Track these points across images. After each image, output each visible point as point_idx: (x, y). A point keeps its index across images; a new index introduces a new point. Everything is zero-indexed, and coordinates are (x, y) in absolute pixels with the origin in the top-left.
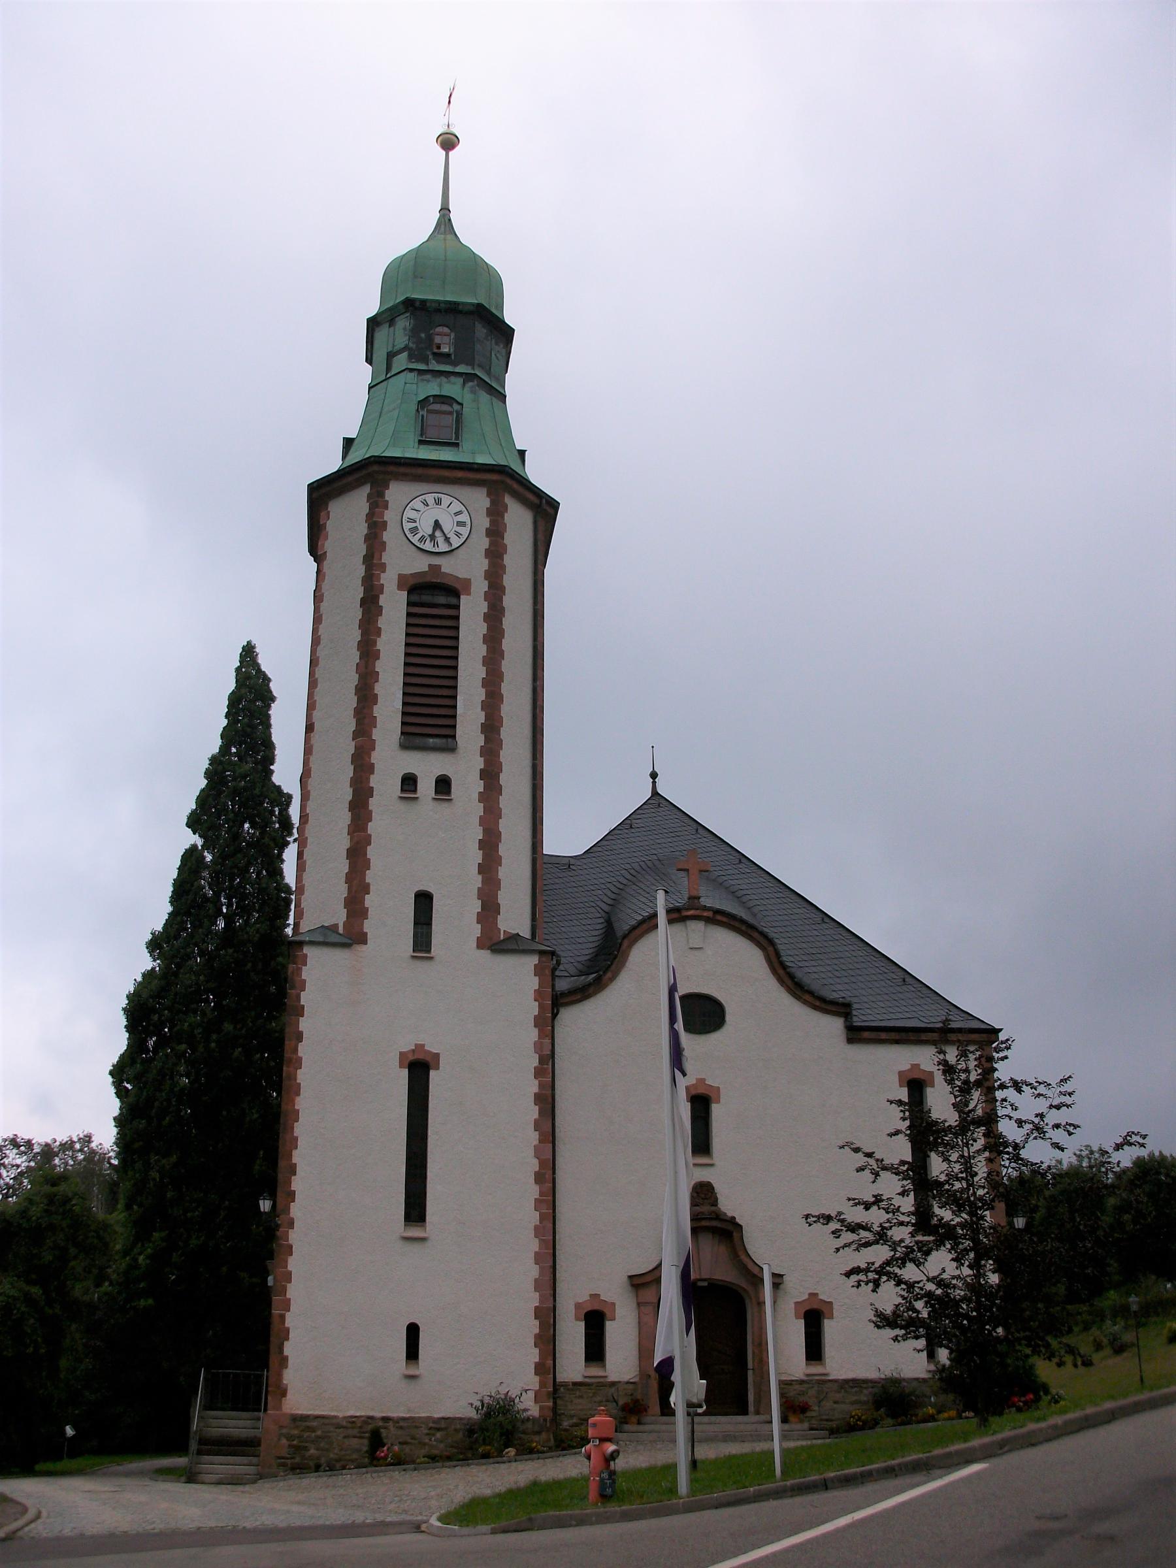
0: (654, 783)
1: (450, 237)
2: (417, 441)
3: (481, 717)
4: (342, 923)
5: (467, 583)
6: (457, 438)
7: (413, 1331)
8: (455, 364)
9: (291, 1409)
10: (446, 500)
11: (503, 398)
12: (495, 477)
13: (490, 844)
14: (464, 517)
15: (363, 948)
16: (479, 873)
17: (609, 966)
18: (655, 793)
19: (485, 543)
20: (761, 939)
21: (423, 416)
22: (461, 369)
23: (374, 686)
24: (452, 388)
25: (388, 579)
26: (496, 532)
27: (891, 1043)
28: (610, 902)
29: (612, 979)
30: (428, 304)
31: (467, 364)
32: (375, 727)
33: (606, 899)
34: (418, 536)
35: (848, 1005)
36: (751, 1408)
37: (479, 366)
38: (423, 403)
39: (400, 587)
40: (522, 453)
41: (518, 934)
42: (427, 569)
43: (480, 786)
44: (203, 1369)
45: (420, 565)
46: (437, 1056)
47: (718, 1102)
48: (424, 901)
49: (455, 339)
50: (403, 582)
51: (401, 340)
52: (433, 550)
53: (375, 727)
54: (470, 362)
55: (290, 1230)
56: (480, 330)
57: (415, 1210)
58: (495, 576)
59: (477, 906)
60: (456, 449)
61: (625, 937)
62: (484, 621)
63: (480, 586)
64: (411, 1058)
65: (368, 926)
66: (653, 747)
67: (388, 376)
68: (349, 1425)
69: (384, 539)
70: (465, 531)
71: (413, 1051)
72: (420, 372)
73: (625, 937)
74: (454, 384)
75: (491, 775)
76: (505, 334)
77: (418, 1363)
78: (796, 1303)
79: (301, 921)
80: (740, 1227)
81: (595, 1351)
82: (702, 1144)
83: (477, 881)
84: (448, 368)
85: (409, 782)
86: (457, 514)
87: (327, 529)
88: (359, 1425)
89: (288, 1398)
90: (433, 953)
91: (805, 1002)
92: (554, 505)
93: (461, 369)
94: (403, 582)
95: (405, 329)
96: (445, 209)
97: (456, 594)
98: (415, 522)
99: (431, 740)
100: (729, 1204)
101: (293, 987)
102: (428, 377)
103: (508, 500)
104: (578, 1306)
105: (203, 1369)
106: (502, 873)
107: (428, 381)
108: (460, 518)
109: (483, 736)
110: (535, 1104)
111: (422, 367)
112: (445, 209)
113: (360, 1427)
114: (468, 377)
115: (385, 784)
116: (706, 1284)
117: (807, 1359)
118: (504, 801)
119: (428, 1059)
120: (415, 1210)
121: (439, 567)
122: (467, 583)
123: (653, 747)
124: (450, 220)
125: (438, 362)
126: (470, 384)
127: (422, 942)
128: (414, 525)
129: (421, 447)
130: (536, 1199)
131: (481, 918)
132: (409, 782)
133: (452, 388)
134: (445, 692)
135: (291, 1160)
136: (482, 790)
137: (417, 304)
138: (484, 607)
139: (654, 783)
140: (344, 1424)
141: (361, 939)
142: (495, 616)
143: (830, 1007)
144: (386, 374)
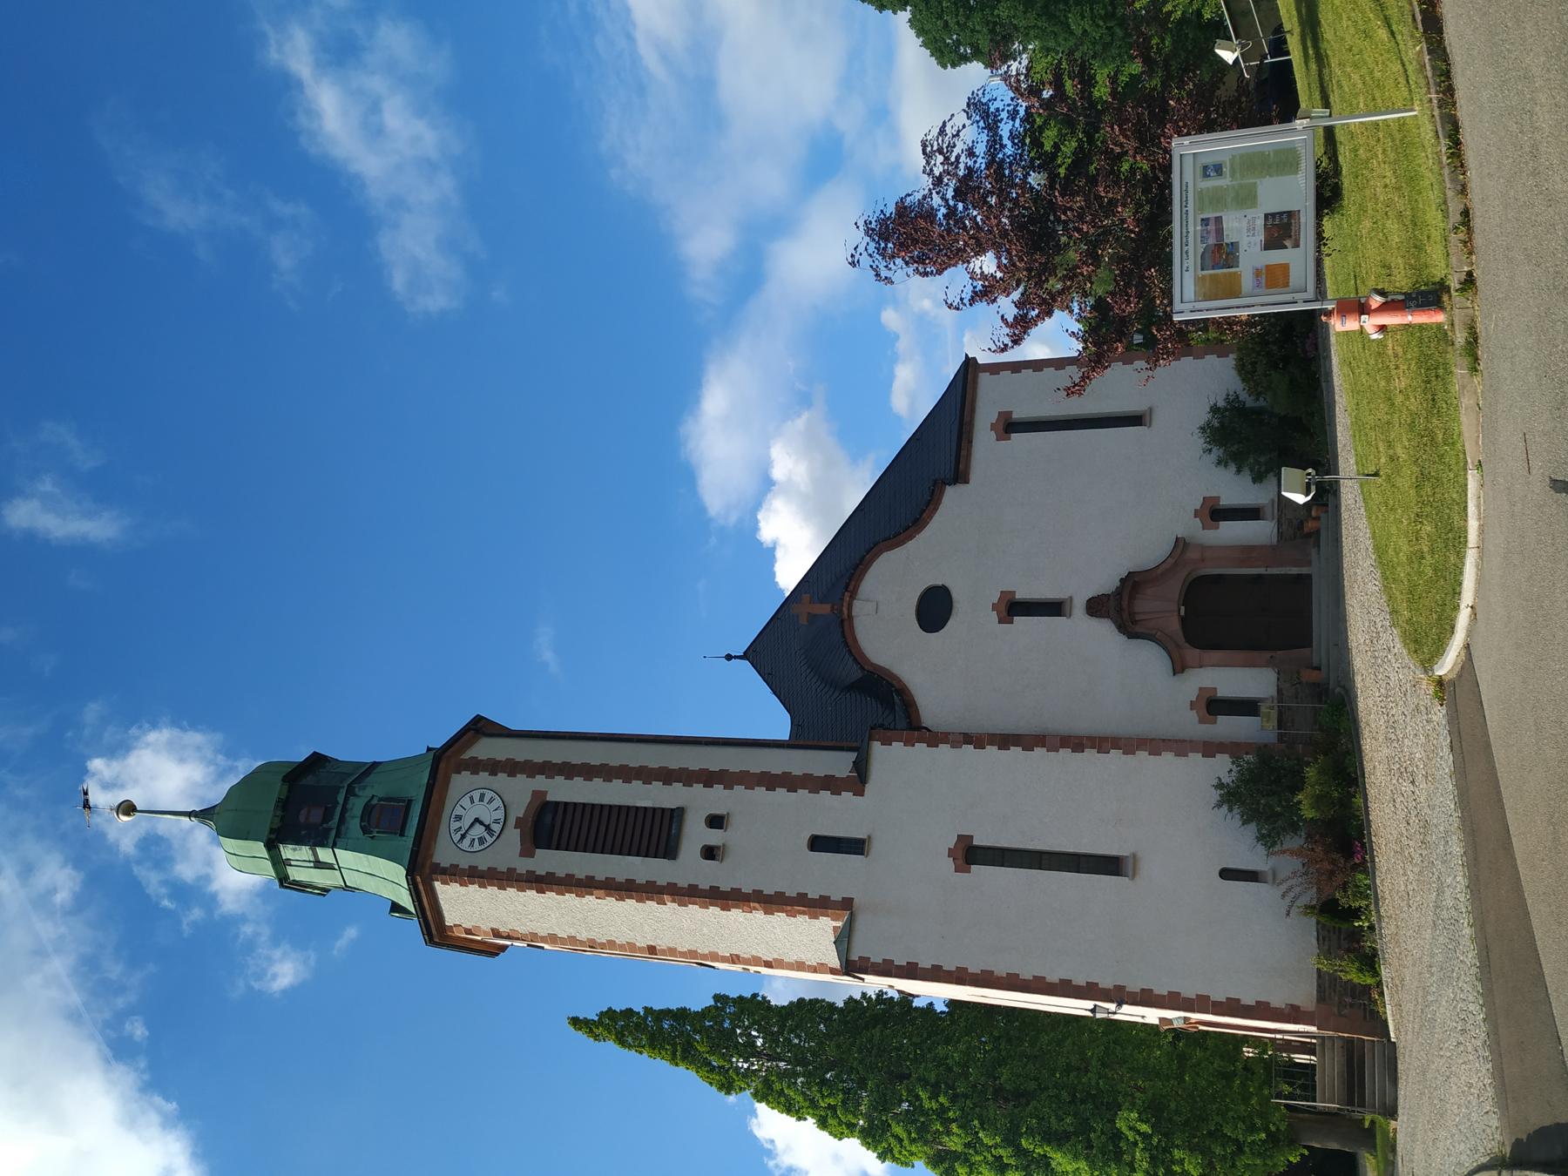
0: (736, 657)
1: (216, 810)
2: (399, 838)
3: (657, 785)
4: (832, 922)
6: (404, 801)
7: (1226, 874)
9: (1312, 1002)
10: (458, 811)
11: (375, 765)
12: (442, 765)
13: (770, 781)
14: (476, 795)
17: (887, 681)
18: (745, 656)
19: (502, 776)
21: (378, 832)
22: (341, 798)
23: (619, 882)
24: (357, 806)
25: (523, 865)
26: (494, 767)
27: (971, 446)
28: (832, 690)
30: (274, 827)
31: (338, 793)
32: (655, 882)
33: (830, 693)
34: (487, 837)
35: (935, 482)
36: (1304, 570)
37: (341, 782)
38: (365, 830)
40: (429, 749)
41: (854, 762)
42: (519, 830)
43: (719, 788)
45: (513, 835)
48: (819, 844)
50: (526, 852)
51: (304, 853)
52: (502, 824)
53: (655, 882)
54: (337, 790)
55: (1127, 989)
56: (309, 780)
57: (1110, 865)
59: (825, 794)
60: (414, 802)
61: (862, 668)
62: (572, 779)
63: (540, 782)
64: (960, 862)
66: (969, 854)
67: (336, 867)
68: (1326, 943)
69: (486, 869)
70: (489, 794)
73: (862, 668)
74: (354, 804)
75: (709, 778)
76: (317, 760)
77: (1261, 872)
78: (1204, 529)
79: (807, 963)
80: (1130, 573)
81: (1246, 707)
82: (1054, 608)
83: (803, 793)
84: (339, 809)
85: (710, 853)
86: (472, 801)
87: (470, 927)
88: (1326, 933)
89: (1300, 1004)
90: (865, 837)
92: (478, 719)
94: (526, 852)
96: (189, 814)
98: (474, 839)
99: (673, 831)
100: (1104, 581)
102: (343, 828)
103: (467, 756)
104: (1201, 721)
106: (797, 772)
107: (348, 828)
108: (476, 799)
109: (674, 784)
111: (333, 833)
112: (189, 814)
113: (1329, 931)
114: (351, 792)
116: (1183, 608)
117: (1258, 519)
118: (734, 769)
120: (1110, 865)
121: (518, 818)
123: (969, 854)
124: (201, 811)
125: (332, 819)
126: (357, 790)
127: (856, 847)
128: (477, 840)
129: (406, 834)
130: (1098, 752)
131: (836, 792)
132: (710, 853)
133: (357, 806)
134: (623, 817)
135: (1083, 986)
136: (722, 786)
137: (273, 836)
138: (559, 779)
139: (736, 657)
140: (1326, 948)
141: (847, 904)
142: (568, 770)
144: (335, 869)
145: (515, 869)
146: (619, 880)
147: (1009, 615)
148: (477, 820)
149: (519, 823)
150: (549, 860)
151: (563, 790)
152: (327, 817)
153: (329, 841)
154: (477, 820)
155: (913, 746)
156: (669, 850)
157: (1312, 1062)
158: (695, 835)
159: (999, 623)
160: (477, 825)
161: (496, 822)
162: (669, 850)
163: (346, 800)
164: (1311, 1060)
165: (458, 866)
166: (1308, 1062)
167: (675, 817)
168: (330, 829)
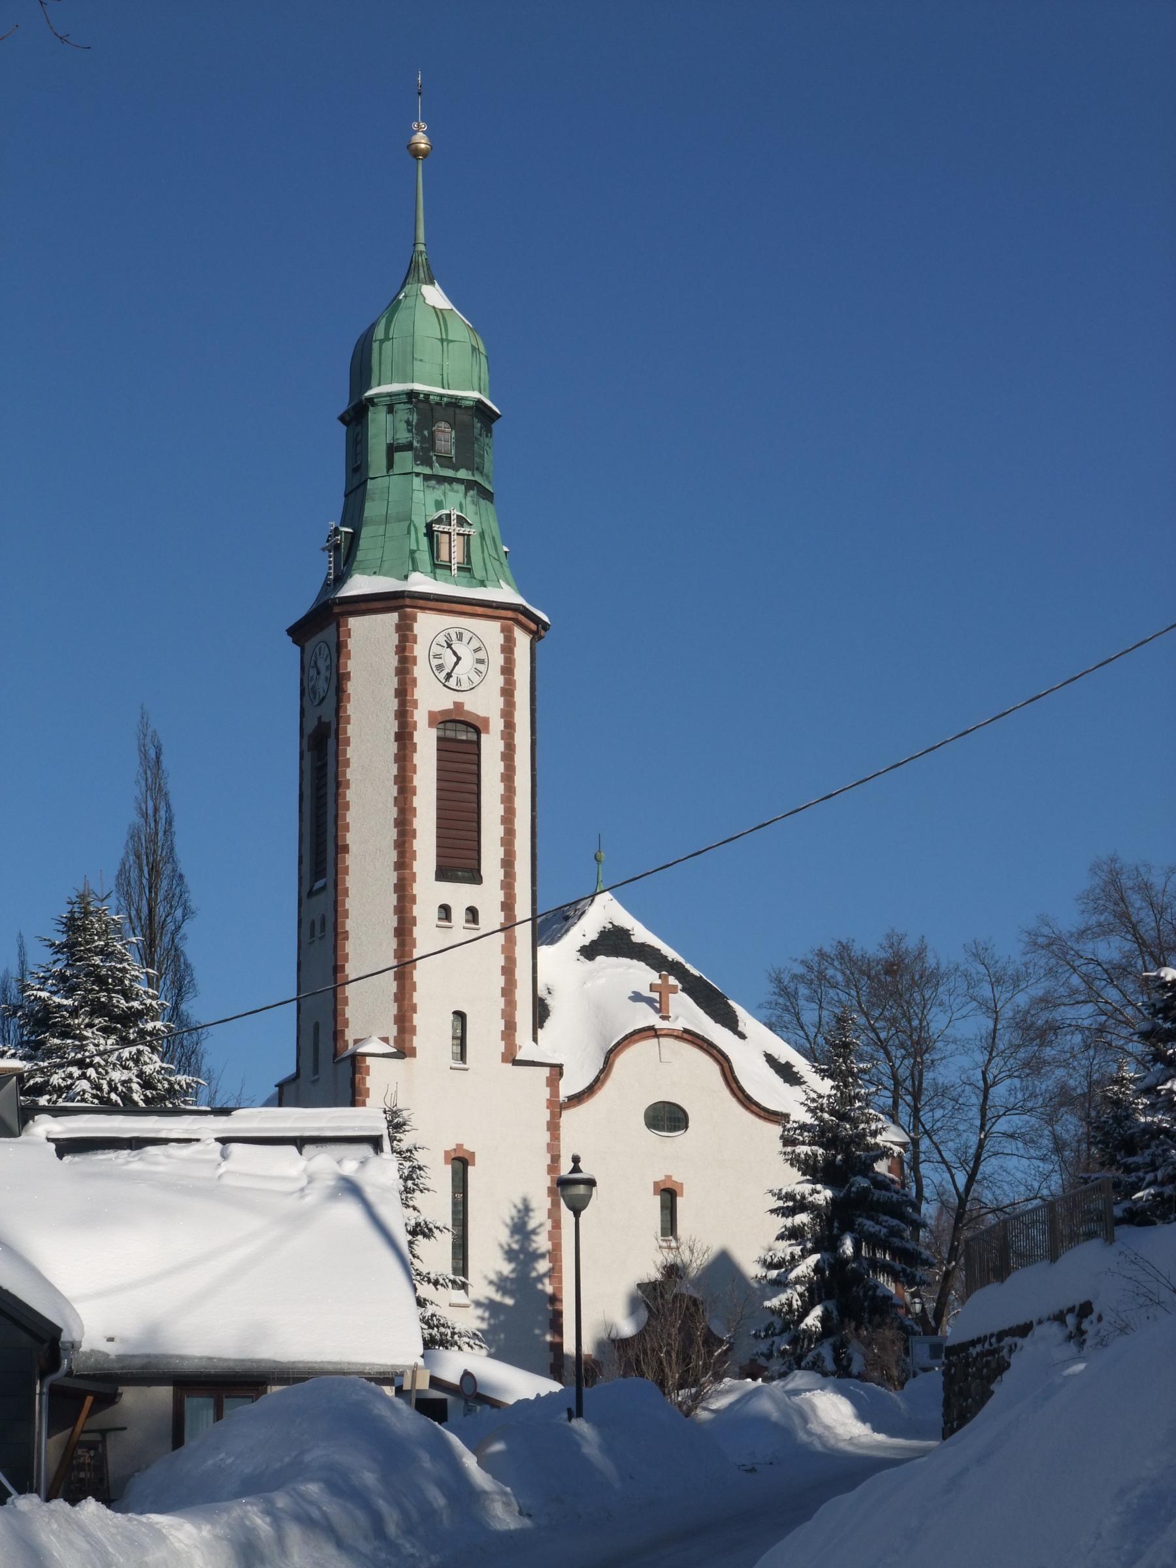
5: (486, 721)
8: (456, 469)
12: (510, 614)
15: (413, 1060)
16: (502, 996)
20: (719, 1057)
22: (463, 474)
25: (420, 717)
29: (599, 1088)
39: (431, 725)
42: (452, 707)
44: (864, 1243)
46: (473, 1154)
47: (682, 1195)
49: (457, 438)
52: (457, 688)
58: (508, 714)
63: (497, 725)
65: (417, 1041)
71: (455, 1150)
72: (427, 478)
74: (457, 492)
84: (449, 473)
85: (445, 911)
91: (752, 1112)
93: (463, 474)
95: (408, 423)
97: (478, 732)
101: (360, 1095)
102: (433, 483)
105: (864, 1243)
110: (548, 1196)
111: (427, 471)
115: (424, 912)
119: (466, 1157)
122: (486, 721)
125: (441, 466)
132: (445, 911)
143: (772, 1117)
145: (416, 708)
146: (415, 757)
147: (664, 1190)
148: (459, 659)
149: (458, 706)
150: (426, 741)
151: (491, 746)
152: (446, 462)
153: (420, 467)
154: (459, 659)
155: (548, 1108)
156: (444, 873)
157: (45, 1390)
158: (459, 895)
159: (503, 1061)
160: (398, 456)
161: (459, 682)
162: (444, 873)
163: (460, 481)
164: (41, 1394)
165: (416, 643)
166: (44, 1397)
167: (474, 876)
168: (431, 466)
